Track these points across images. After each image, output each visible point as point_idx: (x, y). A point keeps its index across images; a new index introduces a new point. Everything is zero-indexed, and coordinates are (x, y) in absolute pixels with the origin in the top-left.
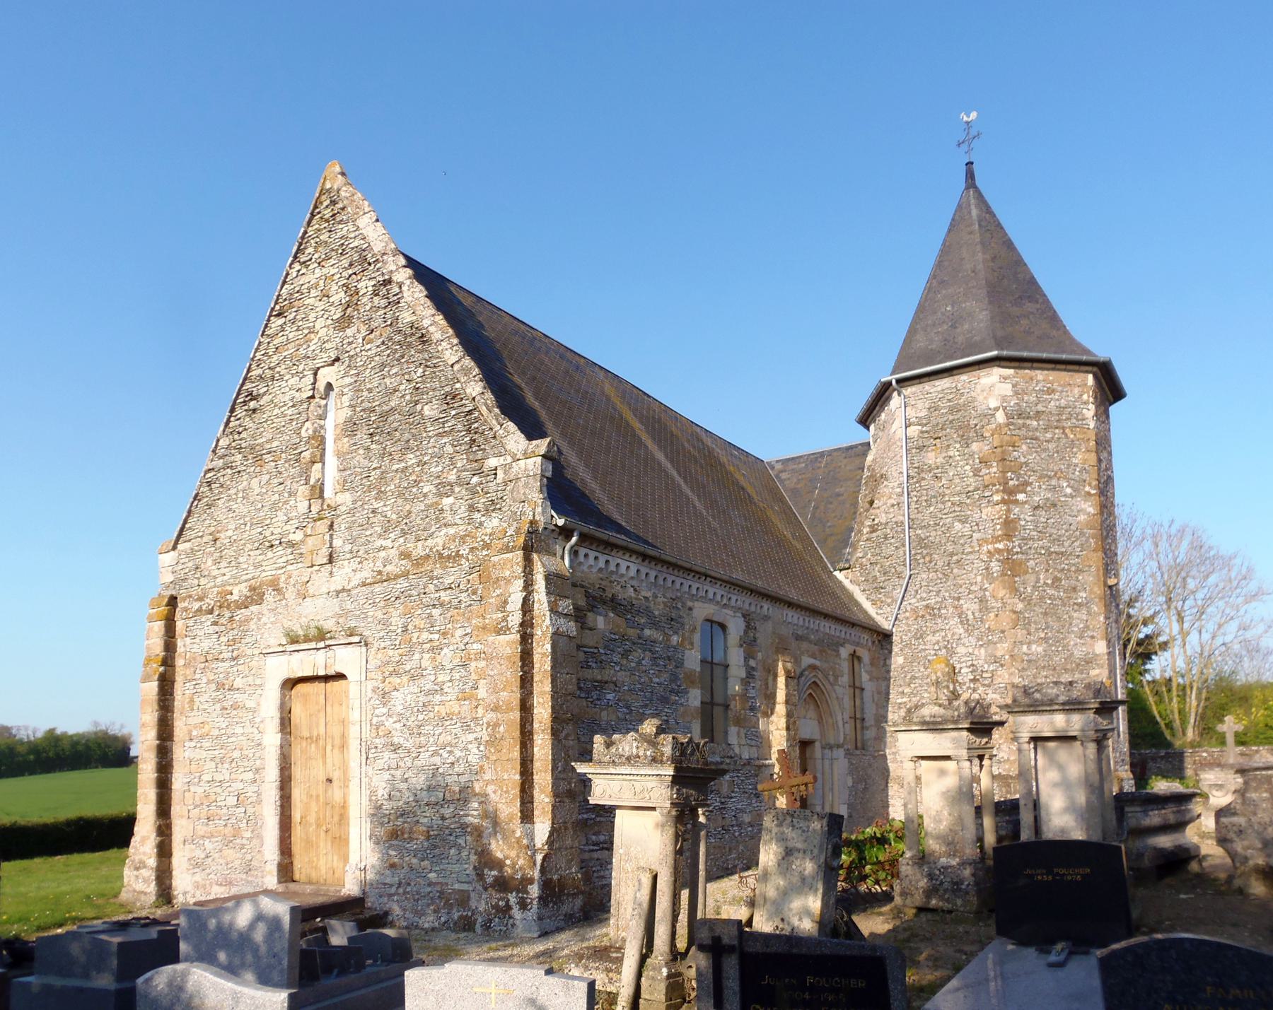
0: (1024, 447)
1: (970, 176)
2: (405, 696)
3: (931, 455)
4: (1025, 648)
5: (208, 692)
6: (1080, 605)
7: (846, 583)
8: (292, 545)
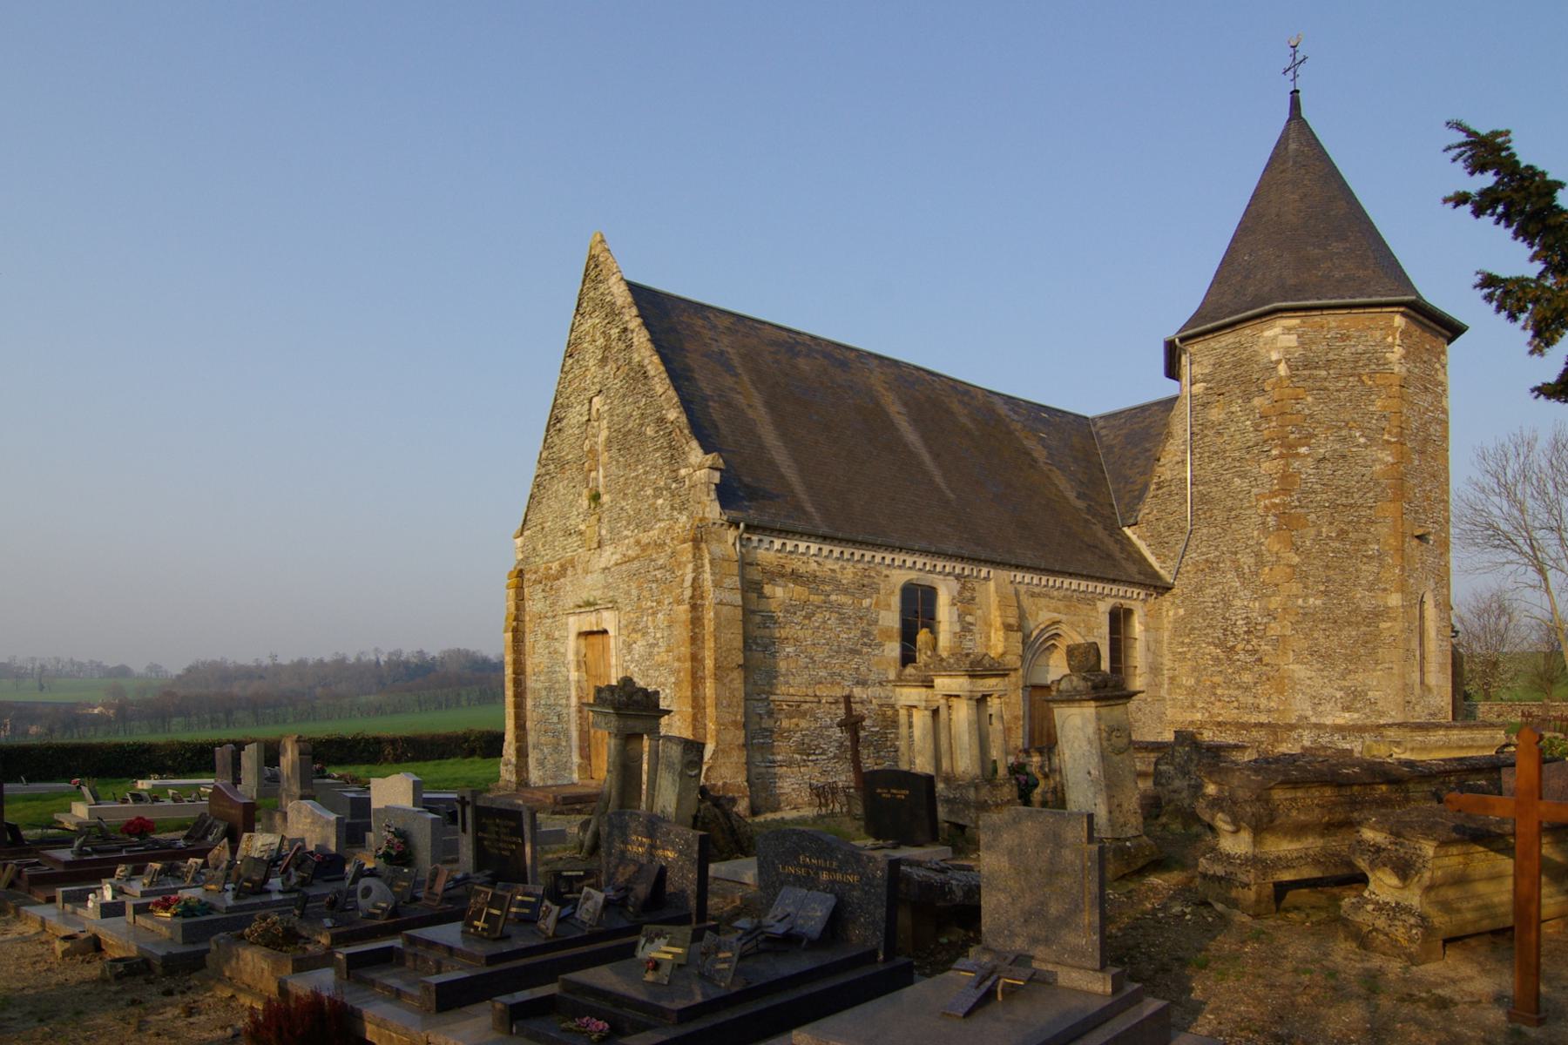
2: (639, 647)
4: (1300, 601)
5: (542, 641)
6: (1370, 557)
7: (1134, 538)
8: (581, 533)
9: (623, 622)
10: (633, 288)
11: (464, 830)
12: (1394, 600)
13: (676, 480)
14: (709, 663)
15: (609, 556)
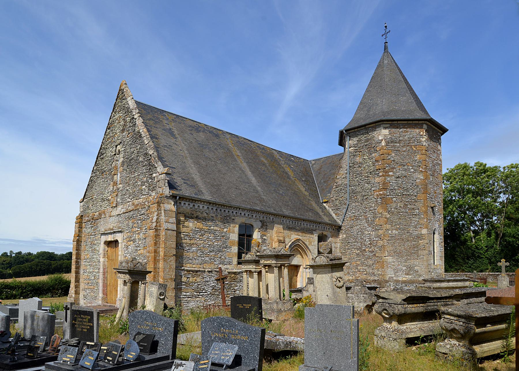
0: (393, 154)
1: (386, 48)
3: (358, 158)
7: (327, 207)
8: (109, 200)
9: (125, 237)
10: (136, 102)
11: (66, 321)
12: (424, 231)
13: (151, 178)
14: (162, 254)
15: (120, 210)
